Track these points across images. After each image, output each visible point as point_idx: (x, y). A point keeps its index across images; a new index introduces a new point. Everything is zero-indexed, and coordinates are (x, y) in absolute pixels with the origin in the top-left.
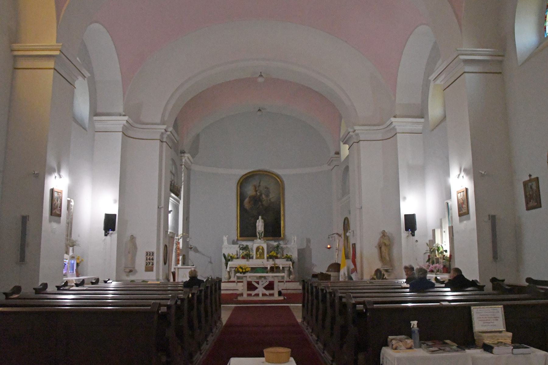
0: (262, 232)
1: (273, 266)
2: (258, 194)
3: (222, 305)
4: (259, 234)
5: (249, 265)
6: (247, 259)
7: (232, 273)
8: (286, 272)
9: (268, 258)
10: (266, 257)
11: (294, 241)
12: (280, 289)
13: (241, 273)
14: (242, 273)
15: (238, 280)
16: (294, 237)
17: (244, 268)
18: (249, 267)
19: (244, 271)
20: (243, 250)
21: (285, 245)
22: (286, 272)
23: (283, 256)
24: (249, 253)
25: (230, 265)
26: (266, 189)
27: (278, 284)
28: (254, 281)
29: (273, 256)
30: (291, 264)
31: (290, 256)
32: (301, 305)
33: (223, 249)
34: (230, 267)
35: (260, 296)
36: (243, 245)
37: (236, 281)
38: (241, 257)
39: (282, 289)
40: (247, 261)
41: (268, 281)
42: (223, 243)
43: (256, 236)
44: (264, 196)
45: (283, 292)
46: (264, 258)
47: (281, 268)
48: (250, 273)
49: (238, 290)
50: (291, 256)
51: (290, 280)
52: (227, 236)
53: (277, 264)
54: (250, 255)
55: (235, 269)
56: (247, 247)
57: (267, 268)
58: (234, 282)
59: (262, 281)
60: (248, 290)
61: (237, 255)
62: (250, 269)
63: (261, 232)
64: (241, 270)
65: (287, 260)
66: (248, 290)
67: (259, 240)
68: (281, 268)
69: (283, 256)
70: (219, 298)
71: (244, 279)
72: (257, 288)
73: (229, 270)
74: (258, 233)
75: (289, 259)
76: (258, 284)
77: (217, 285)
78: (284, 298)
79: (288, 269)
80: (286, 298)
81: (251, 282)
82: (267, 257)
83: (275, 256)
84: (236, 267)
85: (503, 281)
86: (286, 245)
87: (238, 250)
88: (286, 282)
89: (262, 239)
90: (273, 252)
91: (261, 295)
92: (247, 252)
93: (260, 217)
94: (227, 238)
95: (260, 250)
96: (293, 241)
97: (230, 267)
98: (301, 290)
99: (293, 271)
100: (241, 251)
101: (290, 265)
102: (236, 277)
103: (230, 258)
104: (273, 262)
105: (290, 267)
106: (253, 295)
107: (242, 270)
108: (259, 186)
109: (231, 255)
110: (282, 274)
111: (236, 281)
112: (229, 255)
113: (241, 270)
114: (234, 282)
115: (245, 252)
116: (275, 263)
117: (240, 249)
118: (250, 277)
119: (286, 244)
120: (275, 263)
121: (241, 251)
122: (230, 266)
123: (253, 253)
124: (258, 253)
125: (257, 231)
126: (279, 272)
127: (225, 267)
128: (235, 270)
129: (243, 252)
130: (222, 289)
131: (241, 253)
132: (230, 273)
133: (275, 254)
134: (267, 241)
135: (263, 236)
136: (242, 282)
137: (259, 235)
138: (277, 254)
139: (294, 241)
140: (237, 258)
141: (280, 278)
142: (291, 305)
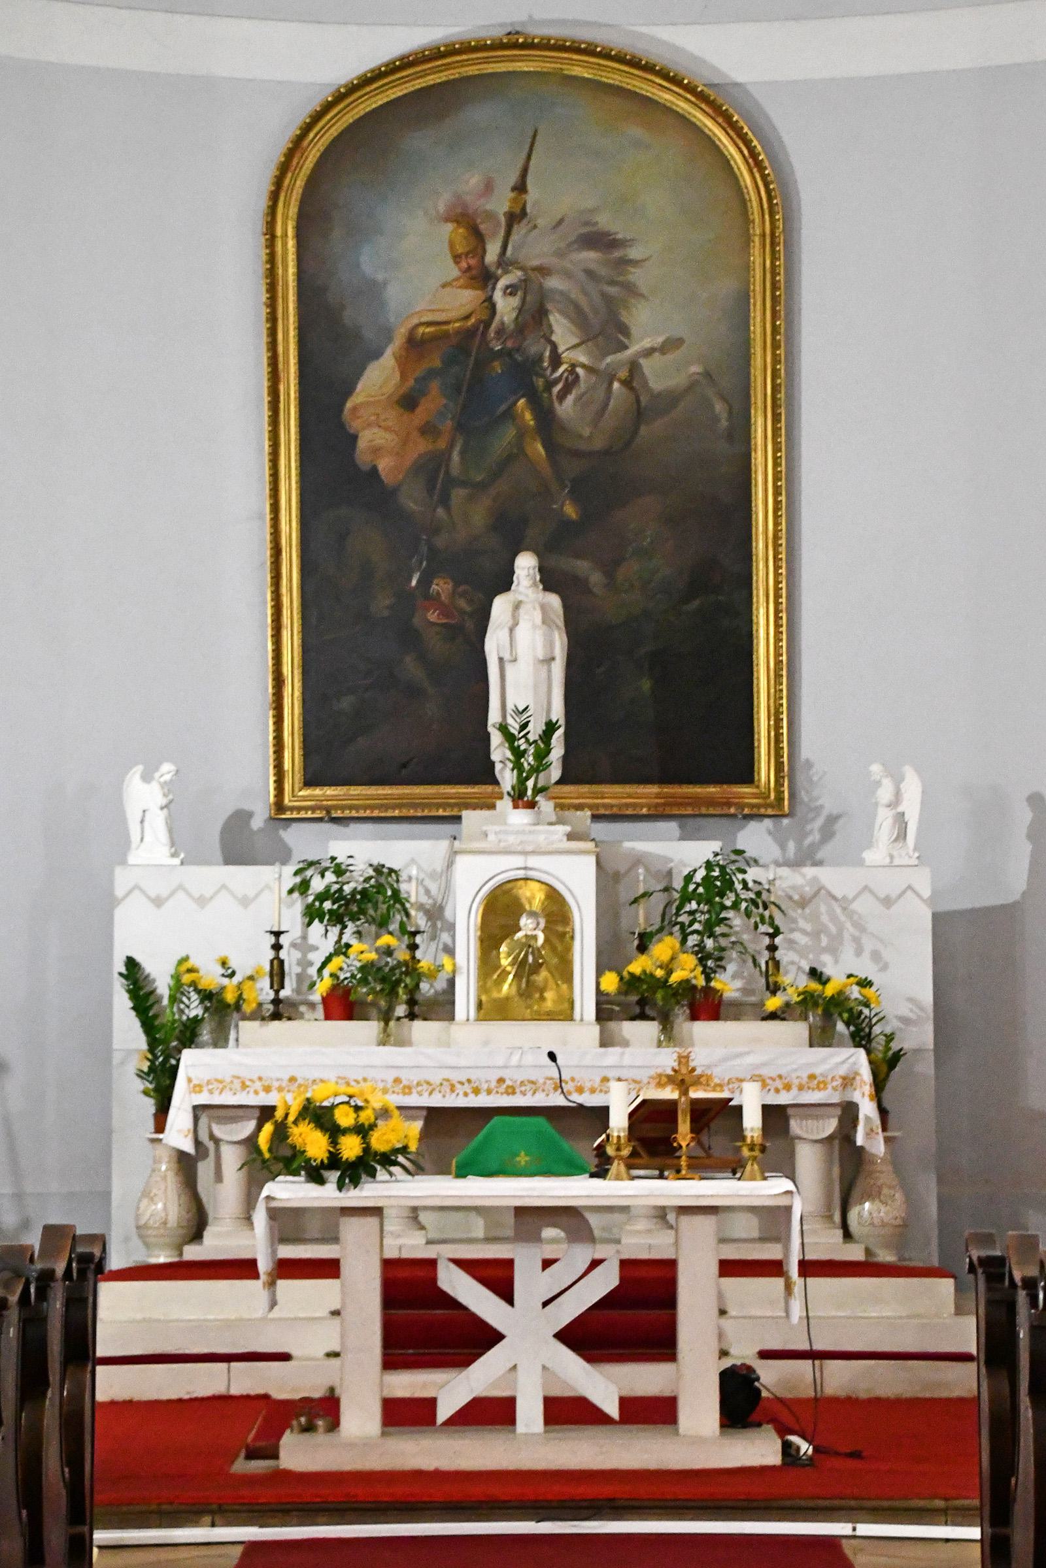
0: (551, 727)
1: (669, 1093)
2: (506, 307)
3: (101, 1536)
4: (519, 754)
5: (408, 1090)
6: (386, 1017)
7: (219, 1177)
8: (808, 1159)
9: (605, 1012)
10: (586, 1005)
11: (901, 821)
12: (743, 1353)
13: (316, 1175)
14: (333, 1176)
15: (289, 1252)
16: (898, 781)
17: (344, 1118)
18: (406, 1111)
19: (351, 1148)
20: (337, 919)
21: (796, 863)
22: (808, 1159)
23: (774, 989)
24: (402, 955)
25: (197, 1089)
26: (590, 257)
27: (720, 1296)
28: (459, 1263)
29: (663, 983)
30: (866, 1074)
31: (855, 992)
32: (975, 1533)
33: (120, 914)
34: (198, 1111)
35: (521, 1427)
36: (339, 871)
37: (264, 1266)
38: (316, 997)
39: (765, 1355)
40: (384, 1040)
41: (612, 1256)
42: (121, 848)
43: (486, 774)
44: (563, 332)
45: (770, 1376)
46: (565, 1013)
47: (752, 1121)
48: (417, 1169)
49: (285, 1357)
50: (865, 983)
51: (855, 1253)
52: (167, 770)
53: (697, 1082)
54: (411, 968)
55: (250, 1126)
56: (380, 888)
57: (602, 1114)
58: (244, 1269)
59: (547, 1264)
60: (390, 1363)
61: (278, 973)
62: (417, 1126)
63: (535, 729)
64: (315, 1144)
65: (821, 1037)
66: (390, 1363)
67: (520, 818)
68: (752, 1121)
69: (774, 989)
70: (73, 1457)
71: (352, 1229)
72: (488, 1337)
73: (188, 1147)
74: (510, 738)
75: (840, 1027)
76: (507, 1295)
77: (56, 1305)
78: (787, 1447)
79: (830, 1126)
80: (805, 1447)
81: (432, 1264)
82: (599, 992)
83: (687, 987)
84: (266, 1112)
85: (146, 1093)
86: (810, 871)
87: (292, 918)
88: (809, 1268)
89: (546, 806)
90: (663, 949)
91: (530, 1415)
92: (386, 940)
93: (525, 564)
94: (167, 788)
95: (526, 923)
96: (884, 821)
97: (198, 1111)
98: (973, 1366)
99: (878, 1147)
100: (322, 938)
101: (848, 1081)
102: (260, 1217)
103: (195, 1009)
104: (667, 1060)
105: (849, 1112)
106: (444, 1412)
107: (334, 1142)
108: (516, 217)
109: (211, 977)
110: (773, 1188)
111: (264, 1266)
112: (184, 970)
113: (315, 1144)
114: (244, 1269)
115: (357, 946)
116: (684, 1059)
117: (312, 914)
118: (414, 1214)
119: (807, 858)
120: (684, 1059)
121: (317, 927)
122: (203, 1099)
123: (450, 951)
124: (504, 948)
125: (494, 716)
126: (735, 1168)
127: (149, 1106)
128: (251, 1142)
129: (342, 949)
130: (101, 1351)
131: (317, 958)
132: (204, 1170)
133: (687, 969)
134: (601, 830)
135: (555, 773)
136: (328, 1269)
137: (518, 766)
138: (710, 961)
139: (901, 821)
140: (280, 1011)
141: (746, 1227)
142: (865, 1529)
